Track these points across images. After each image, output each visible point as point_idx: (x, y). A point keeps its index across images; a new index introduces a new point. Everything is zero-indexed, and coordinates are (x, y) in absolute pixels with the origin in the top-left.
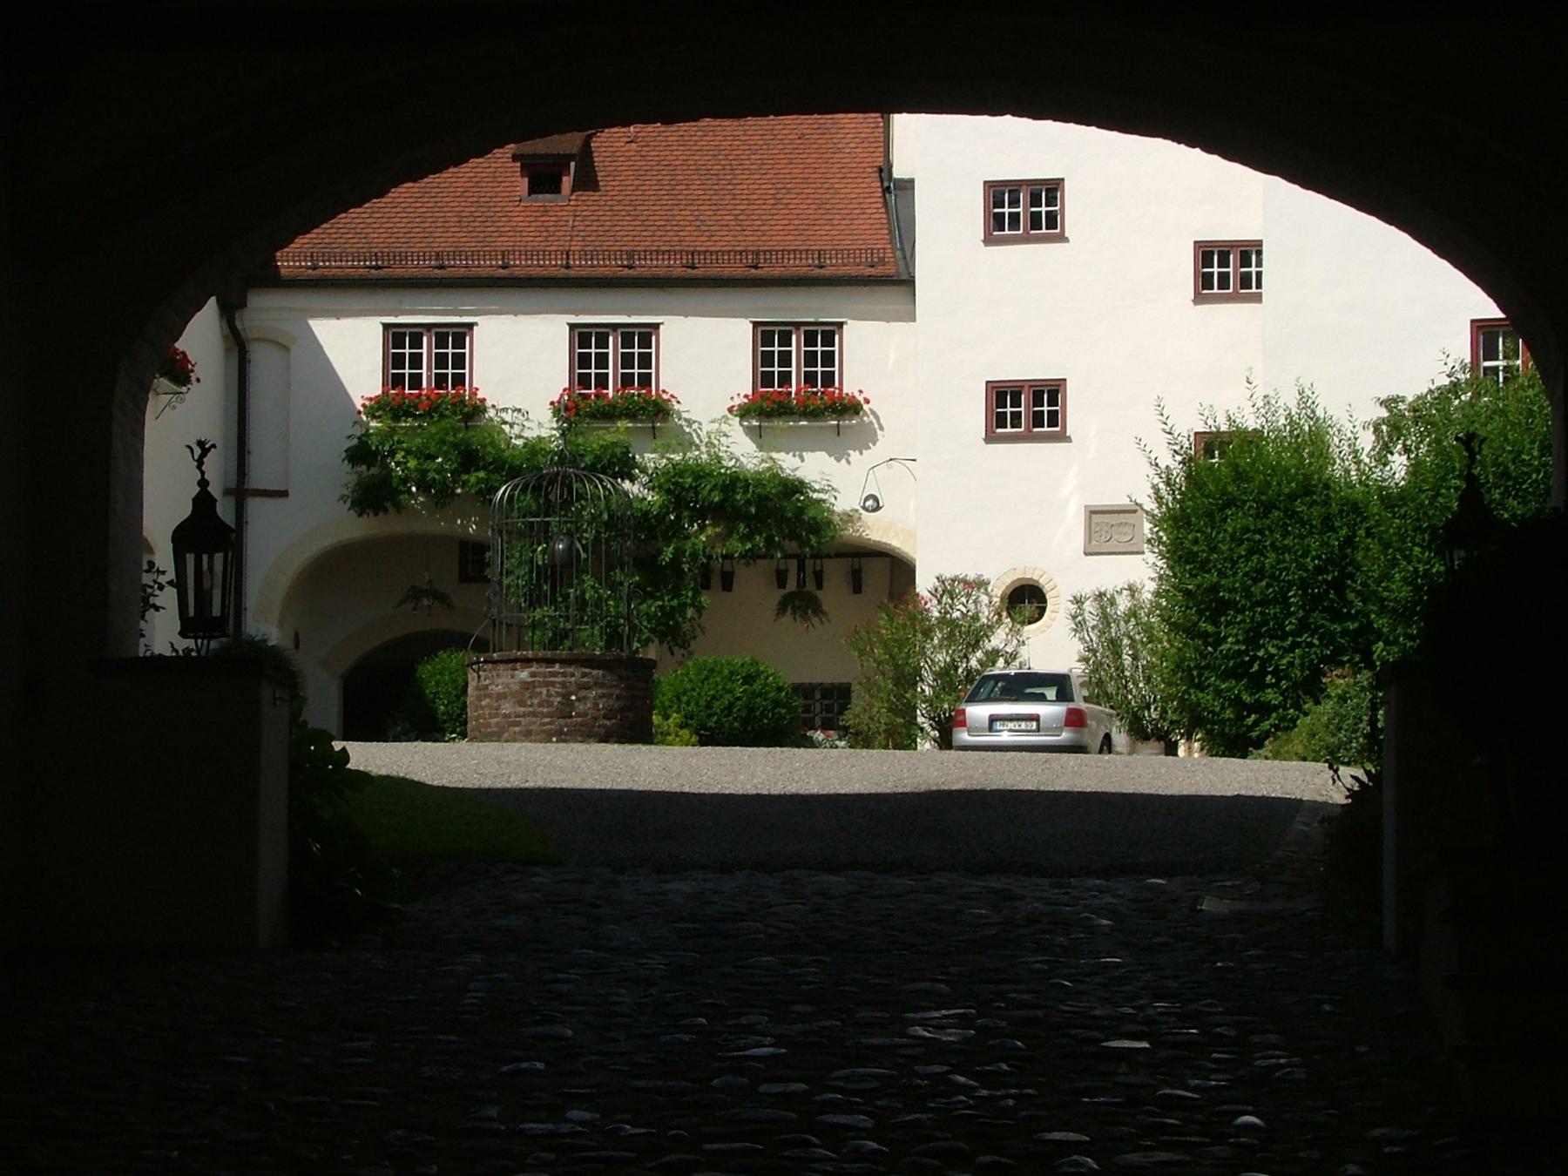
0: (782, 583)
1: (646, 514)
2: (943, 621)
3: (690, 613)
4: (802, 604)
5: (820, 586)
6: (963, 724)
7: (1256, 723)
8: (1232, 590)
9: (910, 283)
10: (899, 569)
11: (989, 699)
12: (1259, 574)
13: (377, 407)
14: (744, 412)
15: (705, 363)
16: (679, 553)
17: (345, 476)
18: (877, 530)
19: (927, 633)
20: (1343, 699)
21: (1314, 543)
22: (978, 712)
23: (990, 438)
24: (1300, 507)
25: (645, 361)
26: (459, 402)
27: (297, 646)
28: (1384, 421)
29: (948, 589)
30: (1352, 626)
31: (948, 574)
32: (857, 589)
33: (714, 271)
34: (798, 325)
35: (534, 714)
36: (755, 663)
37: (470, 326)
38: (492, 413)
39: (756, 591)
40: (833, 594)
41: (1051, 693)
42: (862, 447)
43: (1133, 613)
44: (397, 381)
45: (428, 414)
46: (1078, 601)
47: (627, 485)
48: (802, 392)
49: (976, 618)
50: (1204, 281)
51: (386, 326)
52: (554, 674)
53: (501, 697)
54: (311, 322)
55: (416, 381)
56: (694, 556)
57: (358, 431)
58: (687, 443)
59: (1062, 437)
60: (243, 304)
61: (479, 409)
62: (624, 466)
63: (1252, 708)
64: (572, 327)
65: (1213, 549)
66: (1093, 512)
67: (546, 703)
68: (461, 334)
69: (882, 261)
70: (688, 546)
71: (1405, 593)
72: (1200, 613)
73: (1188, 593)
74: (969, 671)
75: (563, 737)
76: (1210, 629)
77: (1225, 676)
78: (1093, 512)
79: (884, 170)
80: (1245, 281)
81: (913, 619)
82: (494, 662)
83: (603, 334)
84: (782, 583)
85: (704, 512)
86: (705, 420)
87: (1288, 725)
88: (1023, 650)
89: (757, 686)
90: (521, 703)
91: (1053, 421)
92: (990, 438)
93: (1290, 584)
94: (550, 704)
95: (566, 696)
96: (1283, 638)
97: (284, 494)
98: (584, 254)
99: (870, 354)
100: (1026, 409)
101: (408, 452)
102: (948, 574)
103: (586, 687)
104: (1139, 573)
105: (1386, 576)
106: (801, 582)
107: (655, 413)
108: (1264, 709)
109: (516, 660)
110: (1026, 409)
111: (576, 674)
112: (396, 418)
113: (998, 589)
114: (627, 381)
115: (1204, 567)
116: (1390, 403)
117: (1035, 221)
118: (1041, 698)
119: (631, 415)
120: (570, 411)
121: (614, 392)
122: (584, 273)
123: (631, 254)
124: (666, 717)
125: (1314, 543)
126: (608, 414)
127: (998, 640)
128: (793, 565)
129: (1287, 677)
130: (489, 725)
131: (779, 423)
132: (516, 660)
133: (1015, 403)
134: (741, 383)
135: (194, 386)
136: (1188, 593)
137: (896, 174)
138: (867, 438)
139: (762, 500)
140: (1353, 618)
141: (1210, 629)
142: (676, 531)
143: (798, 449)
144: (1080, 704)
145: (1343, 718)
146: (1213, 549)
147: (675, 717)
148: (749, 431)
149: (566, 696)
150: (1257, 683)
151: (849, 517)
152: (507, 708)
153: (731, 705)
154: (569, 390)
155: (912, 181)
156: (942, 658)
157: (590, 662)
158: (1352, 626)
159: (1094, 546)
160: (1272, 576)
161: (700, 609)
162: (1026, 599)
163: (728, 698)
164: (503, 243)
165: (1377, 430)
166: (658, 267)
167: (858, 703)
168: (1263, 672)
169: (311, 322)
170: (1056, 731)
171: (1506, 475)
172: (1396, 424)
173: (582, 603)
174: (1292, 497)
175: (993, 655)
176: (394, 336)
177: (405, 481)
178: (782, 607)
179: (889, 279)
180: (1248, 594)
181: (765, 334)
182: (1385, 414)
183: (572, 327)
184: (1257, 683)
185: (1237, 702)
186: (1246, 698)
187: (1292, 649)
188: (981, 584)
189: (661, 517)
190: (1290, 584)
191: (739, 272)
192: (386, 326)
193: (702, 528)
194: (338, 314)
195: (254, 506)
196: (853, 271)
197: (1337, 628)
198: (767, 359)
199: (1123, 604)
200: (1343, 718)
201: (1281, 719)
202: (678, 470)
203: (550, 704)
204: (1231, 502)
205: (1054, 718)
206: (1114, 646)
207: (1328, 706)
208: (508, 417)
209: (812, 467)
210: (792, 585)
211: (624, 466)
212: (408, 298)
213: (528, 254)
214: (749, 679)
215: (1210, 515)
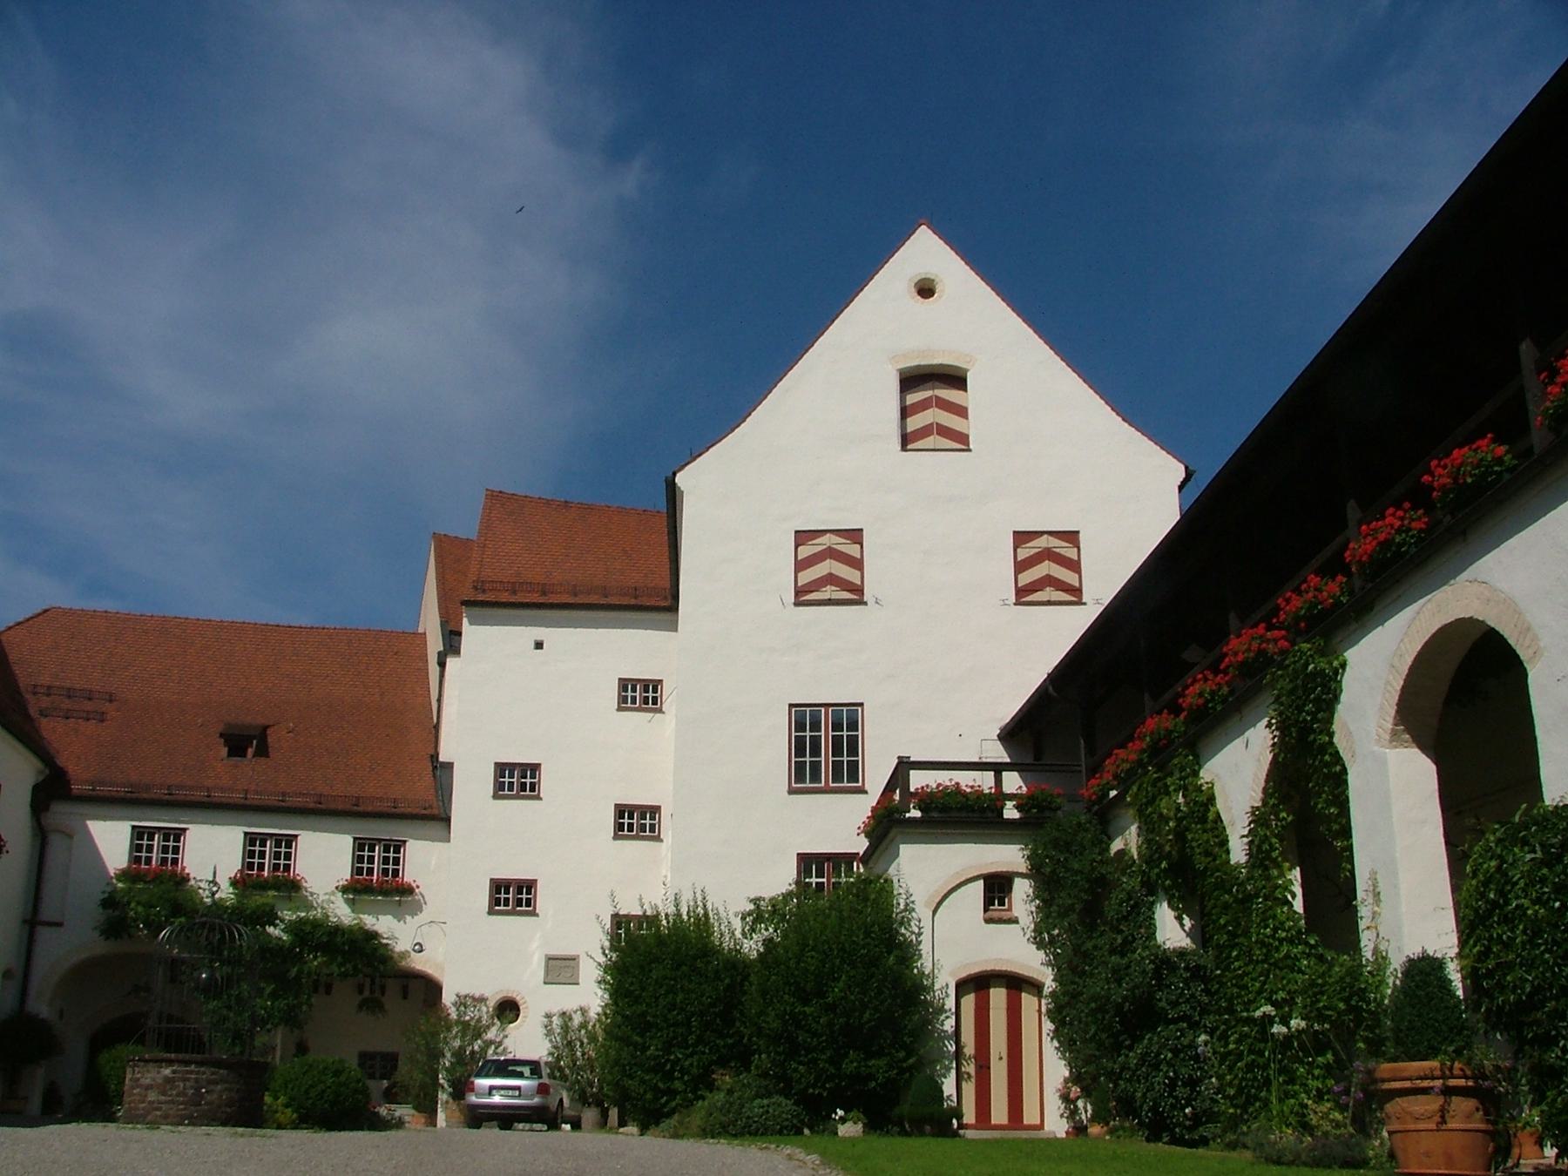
0: (361, 992)
1: (281, 948)
2: (458, 1022)
4: (372, 1005)
6: (472, 1090)
7: (667, 1102)
9: (448, 820)
10: (432, 988)
11: (487, 1076)
12: (673, 1006)
13: (124, 875)
14: (344, 890)
15: (323, 860)
16: (300, 972)
18: (419, 963)
19: (449, 1029)
20: (730, 1092)
22: (483, 1083)
23: (491, 912)
24: (699, 964)
26: (174, 873)
28: (750, 914)
31: (463, 993)
33: (333, 806)
34: (380, 840)
35: (172, 1102)
37: (184, 830)
38: (192, 882)
41: (526, 1070)
42: (413, 914)
43: (583, 1025)
44: (137, 860)
45: (153, 880)
46: (548, 1016)
47: (270, 929)
48: (377, 881)
50: (619, 827)
51: (134, 827)
52: (191, 1072)
53: (148, 1087)
54: (89, 823)
55: (149, 860)
56: (309, 974)
57: (109, 889)
58: (309, 906)
59: (534, 914)
60: (47, 809)
61: (186, 879)
62: (272, 918)
63: (664, 1093)
64: (246, 834)
65: (643, 989)
66: (550, 959)
67: (183, 1094)
68: (179, 834)
69: (431, 807)
70: (306, 970)
73: (625, 1017)
74: (473, 1052)
76: (638, 1039)
78: (550, 959)
79: (434, 757)
80: (643, 828)
81: (440, 1019)
82: (147, 1061)
84: (361, 992)
85: (316, 949)
86: (321, 893)
88: (507, 1042)
89: (343, 1078)
91: (528, 904)
92: (491, 912)
94: (185, 1095)
95: (198, 1090)
97: (59, 925)
99: (421, 859)
100: (513, 896)
101: (138, 903)
104: (589, 996)
106: (372, 991)
107: (291, 887)
108: (672, 1093)
109: (162, 1061)
110: (513, 896)
111: (207, 1073)
112: (134, 882)
113: (492, 1003)
114: (276, 867)
115: (637, 1000)
117: (523, 787)
118: (520, 1075)
121: (269, 878)
122: (256, 803)
124: (276, 1098)
126: (263, 886)
127: (491, 1034)
128: (368, 980)
129: (688, 1073)
130: (137, 1109)
132: (162, 1061)
134: (344, 873)
136: (625, 1017)
137: (441, 759)
138: (416, 909)
140: (731, 1037)
142: (299, 958)
143: (376, 913)
144: (545, 1080)
145: (731, 1104)
148: (347, 901)
149: (198, 1090)
150: (668, 1076)
151: (404, 955)
154: (241, 871)
156: (457, 1043)
157: (219, 1064)
159: (550, 979)
160: (682, 1009)
161: (310, 1006)
162: (508, 1009)
163: (321, 1087)
165: (743, 918)
167: (403, 1067)
168: (673, 1070)
169: (89, 823)
171: (843, 950)
172: (758, 914)
173: (239, 999)
174: (695, 958)
175: (489, 1043)
177: (135, 920)
178: (360, 1007)
179: (434, 815)
181: (359, 844)
182: (752, 907)
183: (246, 834)
184: (668, 1076)
185: (655, 1089)
186: (661, 1085)
187: (691, 1055)
188: (482, 1000)
191: (348, 807)
193: (315, 958)
194: (105, 818)
196: (415, 811)
197: (720, 1042)
198: (360, 859)
199: (577, 1019)
200: (731, 1104)
202: (301, 922)
203: (185, 1095)
205: (527, 1088)
207: (720, 1097)
208: (202, 885)
209: (383, 924)
210: (367, 993)
211: (272, 918)
213: (222, 790)
214: (337, 1073)
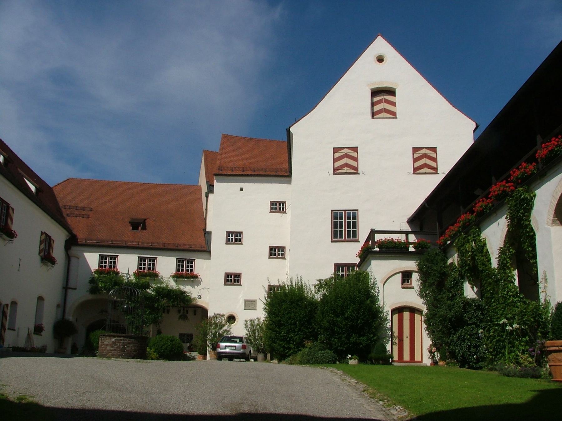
2: (214, 323)
3: (160, 318)
4: (184, 317)
5: (187, 313)
8: (284, 321)
9: (210, 252)
10: (205, 311)
11: (224, 342)
12: (290, 318)
13: (97, 272)
15: (166, 266)
17: (89, 286)
18: (200, 302)
19: (211, 326)
20: (310, 348)
21: (302, 312)
22: (223, 344)
23: (225, 284)
25: (153, 265)
26: (114, 272)
27: (77, 321)
28: (317, 285)
29: (216, 316)
30: (310, 330)
32: (195, 314)
34: (186, 259)
35: (115, 350)
36: (173, 337)
37: (117, 256)
39: (174, 314)
40: (190, 315)
41: (238, 340)
42: (198, 285)
43: (258, 325)
45: (107, 274)
47: (148, 290)
48: (186, 274)
49: (221, 323)
50: (271, 254)
51: (100, 255)
53: (107, 345)
58: (162, 283)
59: (240, 285)
62: (148, 286)
63: (287, 349)
64: (139, 257)
66: (246, 301)
67: (119, 347)
68: (115, 257)
71: (327, 324)
72: (276, 326)
73: (273, 322)
75: (123, 357)
76: (278, 330)
77: (281, 340)
78: (246, 301)
80: (279, 255)
83: (145, 259)
87: (295, 353)
89: (174, 343)
90: (112, 347)
91: (238, 282)
92: (225, 284)
93: (297, 321)
95: (124, 346)
96: (295, 332)
97: (76, 289)
98: (142, 242)
99: (200, 266)
100: (233, 279)
102: (216, 313)
103: (129, 344)
104: (260, 314)
105: (322, 320)
106: (183, 313)
108: (290, 349)
110: (233, 279)
111: (127, 340)
112: (101, 274)
114: (150, 269)
115: (277, 316)
116: (320, 280)
117: (236, 240)
118: (236, 342)
119: (150, 276)
120: (138, 274)
121: (147, 273)
123: (152, 243)
124: (151, 349)
125: (302, 312)
126: (145, 275)
127: (225, 328)
128: (182, 309)
129: (295, 342)
131: (180, 279)
133: (231, 277)
134: (173, 271)
135: (56, 265)
137: (207, 230)
138: (199, 283)
139: (176, 295)
141: (278, 330)
143: (184, 285)
145: (311, 353)
146: (280, 312)
147: (153, 350)
148: (174, 281)
149: (124, 346)
150: (289, 343)
151: (194, 299)
152: (108, 348)
153: (167, 347)
154: (137, 270)
155: (211, 232)
156: (214, 331)
158: (310, 330)
159: (246, 308)
163: (166, 346)
164: (126, 239)
165: (315, 287)
166: (157, 246)
168: (290, 340)
170: (240, 350)
171: (351, 298)
172: (320, 285)
174: (298, 301)
176: (101, 257)
179: (205, 251)
180: (287, 322)
181: (179, 261)
185: (284, 347)
186: (286, 346)
187: (297, 335)
188: (223, 315)
189: (155, 298)
190: (297, 321)
191: (174, 247)
192: (100, 255)
194: (90, 252)
195: (70, 291)
198: (179, 266)
199: (256, 322)
201: (294, 351)
202: (159, 288)
204: (284, 301)
205: (238, 346)
206: (254, 332)
209: (187, 288)
210: (181, 313)
212: (104, 249)
214: (172, 341)
215: (279, 304)
